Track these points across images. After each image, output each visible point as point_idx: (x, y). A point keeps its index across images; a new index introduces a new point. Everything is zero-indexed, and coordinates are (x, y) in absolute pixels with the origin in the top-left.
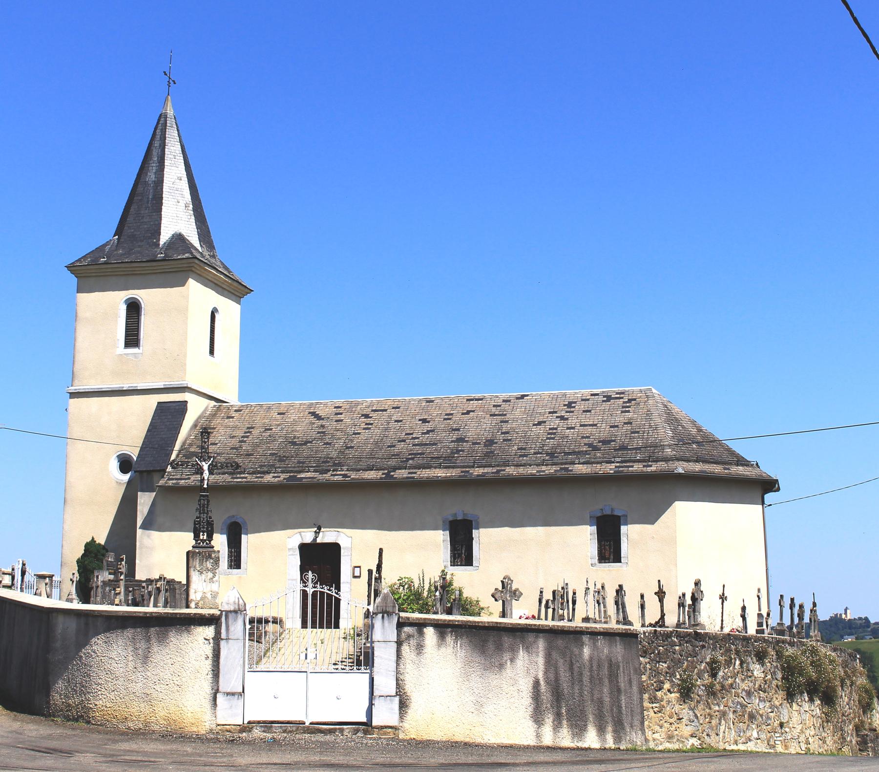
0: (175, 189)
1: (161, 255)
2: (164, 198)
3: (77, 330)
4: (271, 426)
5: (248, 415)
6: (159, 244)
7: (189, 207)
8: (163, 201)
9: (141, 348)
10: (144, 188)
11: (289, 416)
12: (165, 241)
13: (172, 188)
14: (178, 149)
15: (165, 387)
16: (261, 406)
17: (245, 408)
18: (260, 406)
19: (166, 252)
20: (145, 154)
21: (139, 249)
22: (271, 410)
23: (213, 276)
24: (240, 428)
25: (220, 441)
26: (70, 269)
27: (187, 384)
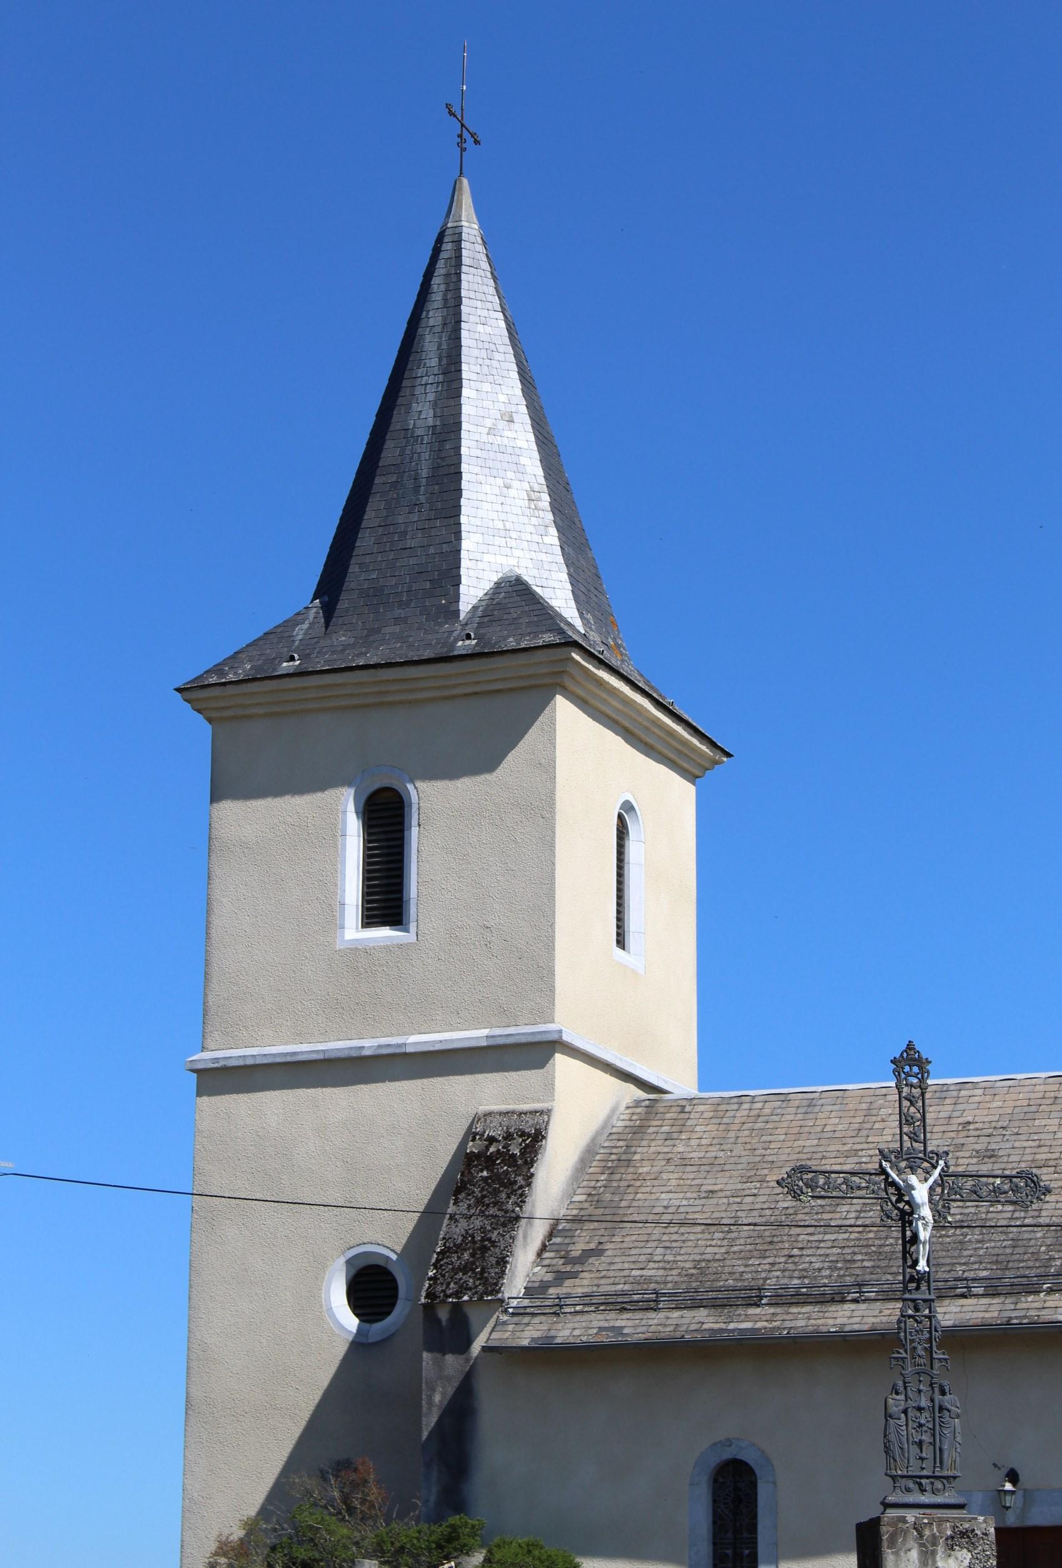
0: (496, 448)
1: (468, 642)
2: (464, 475)
3: (216, 882)
4: (823, 1158)
5: (745, 1126)
6: (457, 612)
7: (539, 499)
8: (464, 484)
9: (413, 927)
10: (403, 449)
11: (877, 1126)
12: (474, 601)
13: (488, 447)
14: (497, 332)
15: (492, 1042)
16: (784, 1098)
17: (735, 1107)
18: (782, 1098)
19: (482, 631)
20: (406, 333)
21: (397, 629)
22: (817, 1109)
23: (620, 707)
24: (727, 1167)
25: (666, 1207)
26: (189, 695)
27: (560, 1032)
